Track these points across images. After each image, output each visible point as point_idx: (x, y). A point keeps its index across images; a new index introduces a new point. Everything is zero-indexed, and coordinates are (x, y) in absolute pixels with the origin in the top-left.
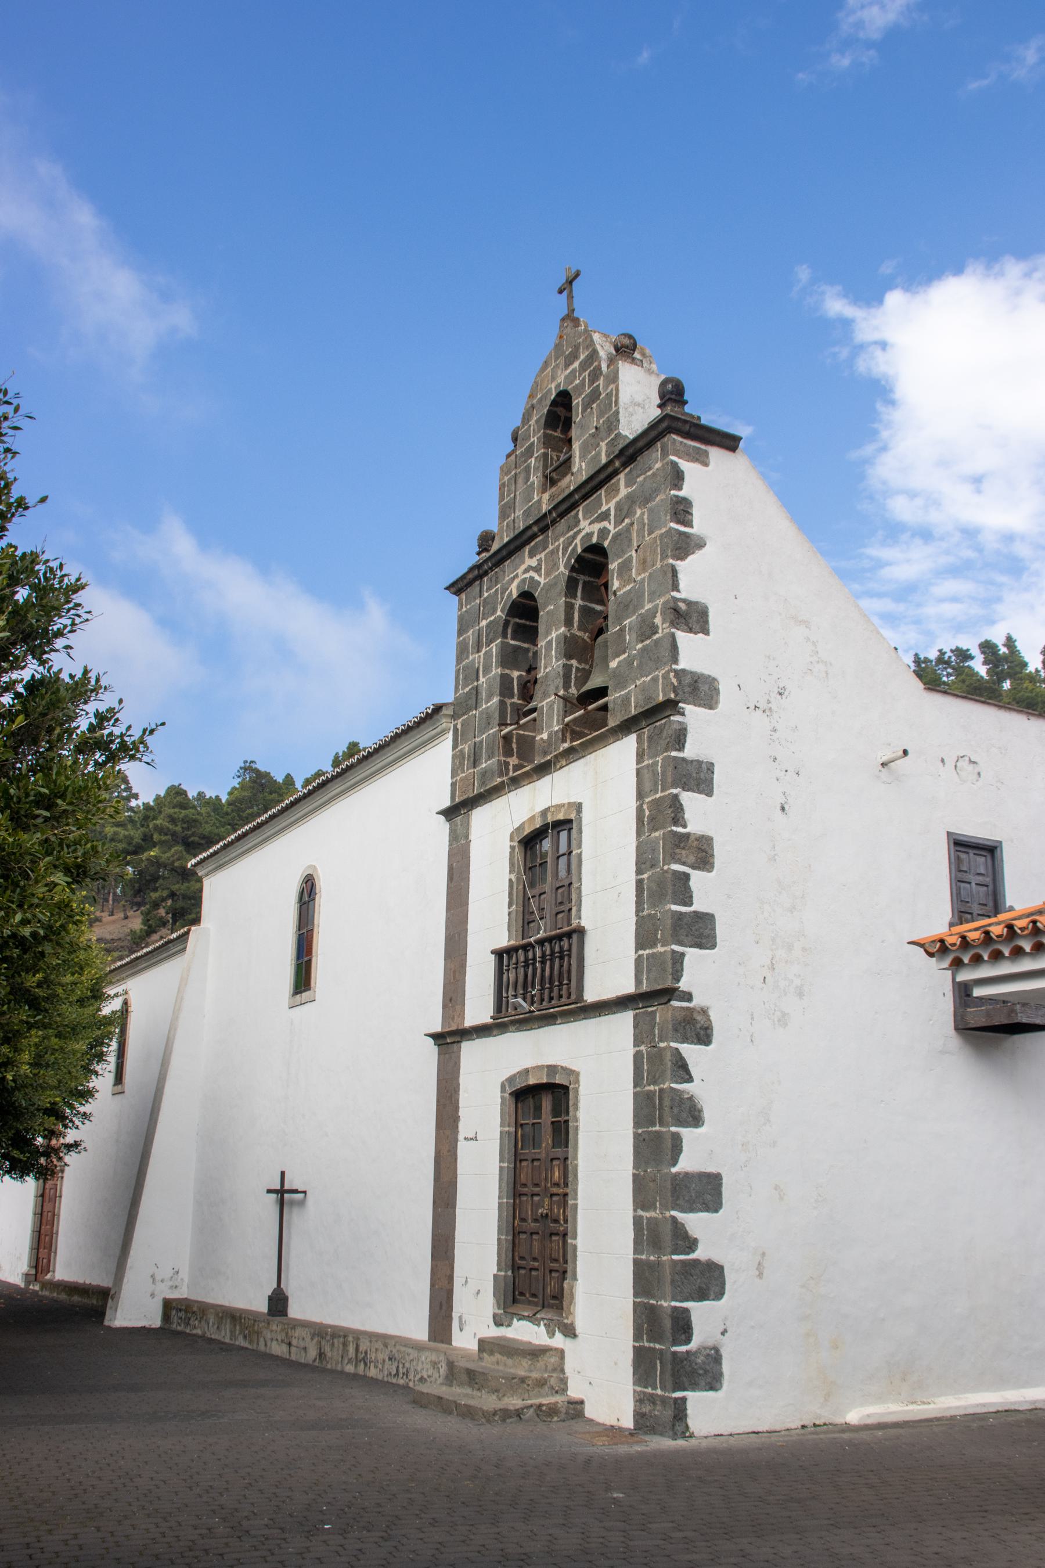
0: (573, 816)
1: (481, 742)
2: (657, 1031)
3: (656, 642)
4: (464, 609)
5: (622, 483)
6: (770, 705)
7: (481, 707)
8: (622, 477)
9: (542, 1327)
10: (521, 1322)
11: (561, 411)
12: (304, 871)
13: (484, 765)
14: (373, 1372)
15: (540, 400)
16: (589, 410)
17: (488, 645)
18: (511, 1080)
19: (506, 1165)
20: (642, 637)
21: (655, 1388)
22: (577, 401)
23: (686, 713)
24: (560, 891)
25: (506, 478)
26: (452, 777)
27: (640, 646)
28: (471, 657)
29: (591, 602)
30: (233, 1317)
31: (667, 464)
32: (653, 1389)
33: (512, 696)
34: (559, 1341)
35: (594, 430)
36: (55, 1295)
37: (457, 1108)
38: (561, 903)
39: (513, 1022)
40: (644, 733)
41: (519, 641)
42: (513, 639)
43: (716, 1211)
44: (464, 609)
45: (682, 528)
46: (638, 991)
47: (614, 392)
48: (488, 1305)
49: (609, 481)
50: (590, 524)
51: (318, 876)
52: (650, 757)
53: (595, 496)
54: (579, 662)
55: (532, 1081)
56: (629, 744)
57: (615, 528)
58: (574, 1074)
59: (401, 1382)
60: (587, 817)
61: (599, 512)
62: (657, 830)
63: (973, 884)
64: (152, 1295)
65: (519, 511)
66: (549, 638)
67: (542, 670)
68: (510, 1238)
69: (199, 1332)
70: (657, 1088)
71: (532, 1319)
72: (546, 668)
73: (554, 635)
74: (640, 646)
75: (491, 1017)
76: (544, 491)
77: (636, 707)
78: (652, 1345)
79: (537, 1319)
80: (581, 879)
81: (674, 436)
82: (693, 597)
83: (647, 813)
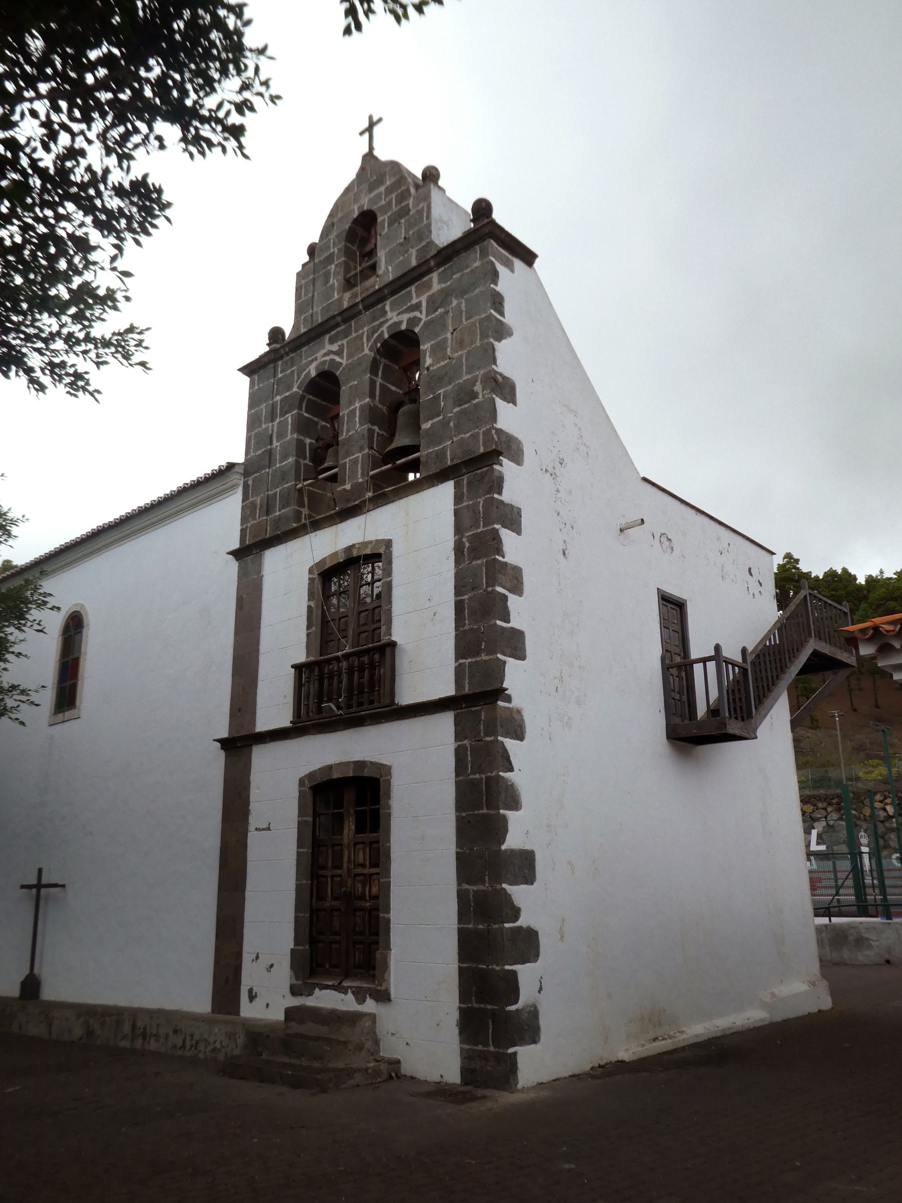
0: (382, 551)
1: (275, 494)
2: (482, 727)
3: (476, 405)
4: (256, 387)
7: (274, 466)
8: (435, 276)
9: (350, 996)
10: (325, 992)
11: (360, 231)
13: (278, 513)
14: (153, 1045)
15: (341, 220)
16: (396, 225)
17: (282, 415)
18: (311, 775)
20: (459, 402)
21: (487, 1045)
22: (383, 219)
23: (503, 464)
24: (363, 614)
25: (303, 282)
26: (241, 525)
28: (264, 426)
29: (388, 382)
31: (487, 262)
33: (305, 459)
34: (370, 1006)
39: (314, 726)
42: (306, 412)
44: (256, 387)
45: (499, 317)
46: (459, 694)
48: (284, 975)
50: (398, 315)
51: (87, 614)
52: (469, 499)
53: (404, 292)
54: (380, 429)
55: (335, 775)
56: (447, 490)
57: (427, 317)
58: (386, 770)
59: (188, 1053)
60: (397, 551)
61: (409, 304)
62: (479, 559)
63: (671, 630)
65: (317, 307)
66: (352, 407)
67: (344, 434)
68: (308, 915)
70: (483, 776)
71: (338, 988)
72: (348, 431)
73: (357, 405)
76: (345, 290)
77: (452, 460)
78: (482, 1006)
82: (506, 374)
83: (467, 545)
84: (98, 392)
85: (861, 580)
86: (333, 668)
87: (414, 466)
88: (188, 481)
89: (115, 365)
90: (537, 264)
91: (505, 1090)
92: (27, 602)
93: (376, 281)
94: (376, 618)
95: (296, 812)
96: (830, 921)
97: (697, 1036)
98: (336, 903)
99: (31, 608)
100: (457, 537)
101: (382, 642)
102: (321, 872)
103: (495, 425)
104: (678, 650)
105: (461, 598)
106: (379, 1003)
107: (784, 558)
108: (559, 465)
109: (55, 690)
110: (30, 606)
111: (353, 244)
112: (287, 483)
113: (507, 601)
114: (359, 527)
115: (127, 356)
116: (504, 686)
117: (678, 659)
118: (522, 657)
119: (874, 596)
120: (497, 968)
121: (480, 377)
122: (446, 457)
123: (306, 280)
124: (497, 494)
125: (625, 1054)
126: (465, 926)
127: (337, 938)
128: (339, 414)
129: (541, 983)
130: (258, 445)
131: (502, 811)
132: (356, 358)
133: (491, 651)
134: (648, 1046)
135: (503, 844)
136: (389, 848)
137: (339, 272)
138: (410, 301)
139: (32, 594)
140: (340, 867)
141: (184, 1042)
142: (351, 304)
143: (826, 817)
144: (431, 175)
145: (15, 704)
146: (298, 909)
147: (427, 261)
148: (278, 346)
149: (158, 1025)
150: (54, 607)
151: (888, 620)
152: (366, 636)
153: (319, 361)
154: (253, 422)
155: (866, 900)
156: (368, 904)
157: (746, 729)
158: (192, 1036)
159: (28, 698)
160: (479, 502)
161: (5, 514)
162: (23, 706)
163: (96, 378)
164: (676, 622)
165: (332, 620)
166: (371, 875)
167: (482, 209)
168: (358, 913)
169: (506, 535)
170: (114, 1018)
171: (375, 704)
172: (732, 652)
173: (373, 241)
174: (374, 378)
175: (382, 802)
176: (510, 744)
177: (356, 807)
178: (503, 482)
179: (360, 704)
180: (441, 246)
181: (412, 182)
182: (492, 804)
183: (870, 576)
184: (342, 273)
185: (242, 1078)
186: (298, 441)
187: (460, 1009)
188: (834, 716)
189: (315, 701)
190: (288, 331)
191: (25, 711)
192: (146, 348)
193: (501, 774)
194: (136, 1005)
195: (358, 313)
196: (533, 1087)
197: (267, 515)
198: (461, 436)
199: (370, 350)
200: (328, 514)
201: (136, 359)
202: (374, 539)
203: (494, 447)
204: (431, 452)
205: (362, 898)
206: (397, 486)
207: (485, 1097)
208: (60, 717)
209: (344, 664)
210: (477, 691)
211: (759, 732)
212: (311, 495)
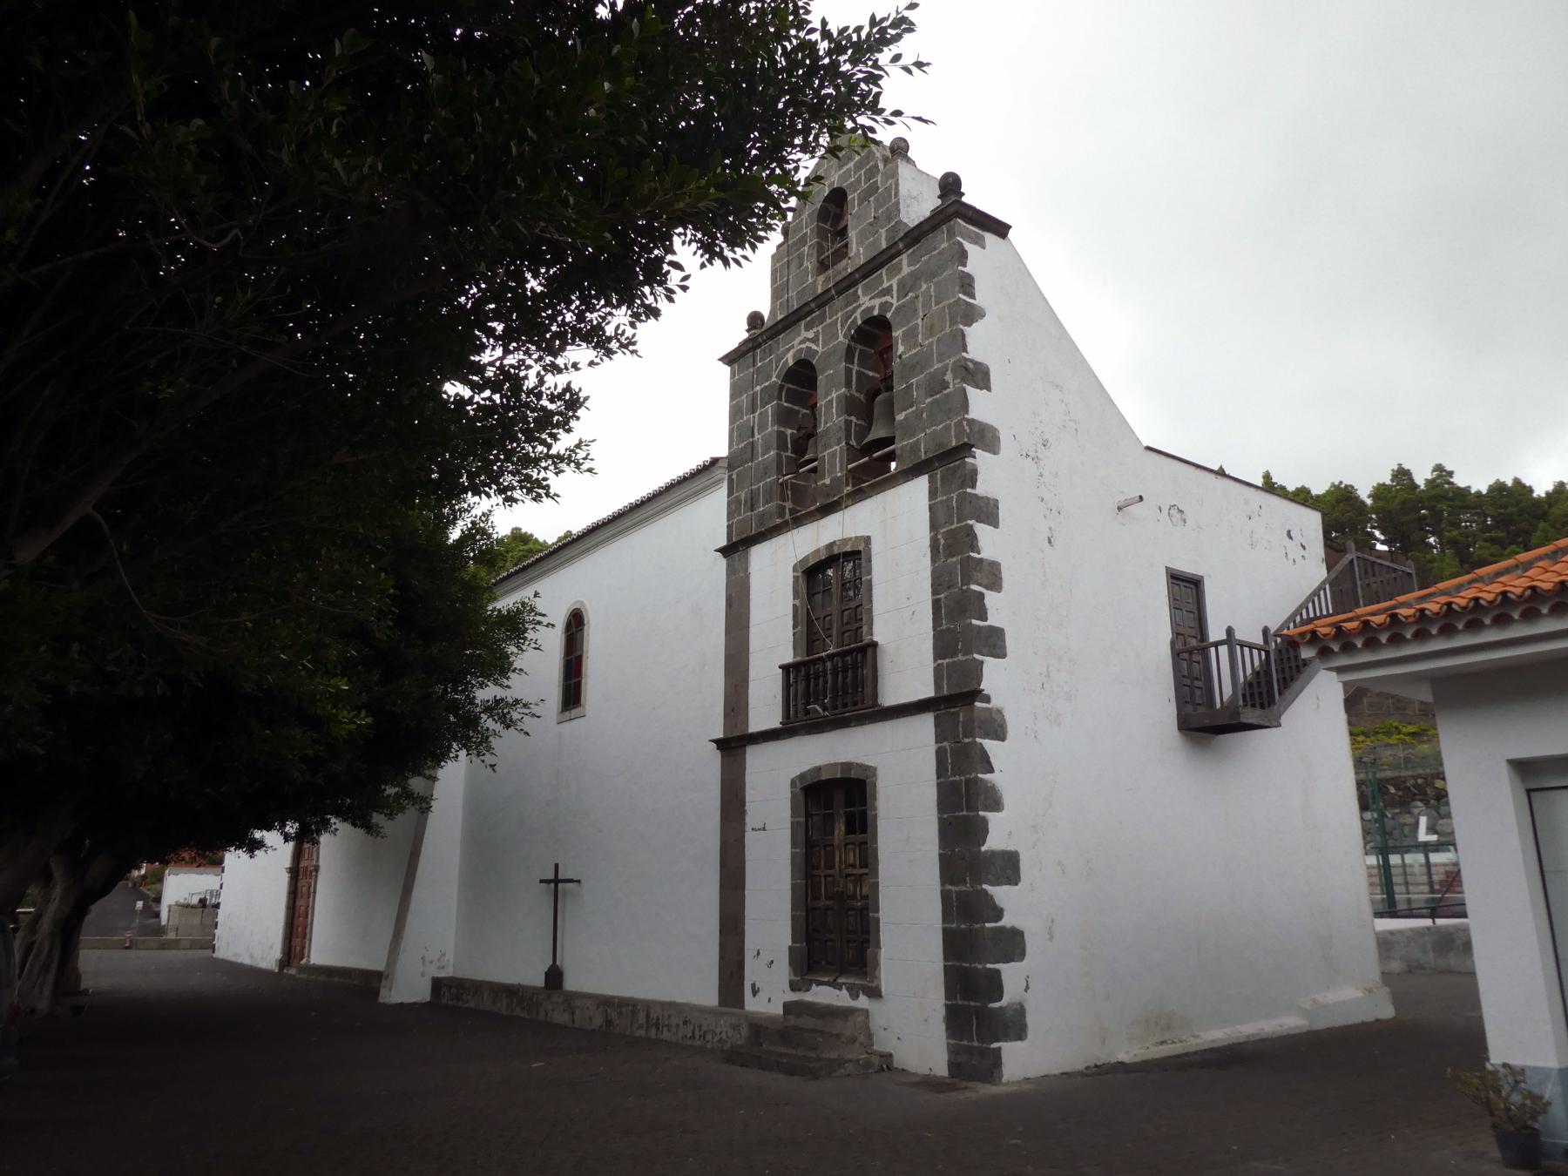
2: (960, 729)
4: (737, 377)
5: (905, 262)
8: (904, 258)
9: (844, 991)
11: (832, 208)
14: (666, 1035)
17: (763, 406)
18: (802, 776)
19: (798, 850)
22: (852, 196)
24: (846, 613)
25: (778, 265)
26: (728, 520)
27: (929, 400)
28: (745, 418)
30: (512, 992)
31: (954, 243)
34: (863, 1002)
35: (873, 219)
36: (313, 977)
38: (847, 624)
40: (937, 474)
41: (791, 403)
43: (1017, 884)
44: (737, 377)
46: (938, 695)
47: (893, 186)
54: (857, 419)
55: (824, 777)
56: (921, 484)
57: (898, 302)
58: (872, 771)
59: (699, 1043)
60: (875, 547)
61: (880, 289)
62: (954, 556)
64: (423, 975)
65: (793, 292)
67: (822, 426)
68: (804, 914)
69: (472, 1004)
70: (963, 778)
71: (835, 985)
72: (826, 423)
73: (834, 395)
74: (929, 400)
75: (781, 723)
76: (819, 274)
77: (925, 453)
78: (966, 1003)
79: (838, 984)
82: (978, 359)
83: (942, 542)
84: (558, 496)
89: (569, 470)
90: (1011, 234)
91: (990, 1083)
93: (848, 264)
94: (859, 617)
95: (789, 813)
96: (1434, 922)
97: (1213, 1041)
98: (829, 903)
99: (527, 629)
102: (815, 872)
103: (966, 416)
104: (1193, 632)
106: (872, 1000)
107: (1434, 471)
108: (1043, 448)
109: (561, 688)
112: (769, 477)
114: (840, 522)
115: (578, 465)
116: (981, 687)
117: (1193, 643)
118: (1003, 655)
119: (1556, 511)
120: (979, 966)
121: (950, 366)
122: (920, 450)
125: (1124, 1056)
127: (832, 936)
128: (816, 404)
130: (741, 437)
131: (981, 813)
132: (831, 346)
133: (968, 652)
136: (876, 849)
137: (812, 254)
140: (832, 867)
141: (693, 1033)
145: (520, 716)
148: (758, 331)
150: (549, 624)
151: (1370, 611)
153: (795, 350)
154: (735, 414)
156: (859, 904)
157: (1266, 717)
158: (700, 1026)
160: (953, 497)
163: (555, 482)
164: (1191, 601)
165: (816, 619)
166: (862, 875)
167: (950, 185)
168: (850, 913)
169: (982, 530)
170: (630, 1008)
174: (850, 366)
176: (989, 745)
178: (977, 475)
179: (845, 705)
180: (912, 225)
185: (742, 1066)
187: (946, 1005)
190: (766, 315)
191: (528, 723)
192: (592, 460)
197: (752, 511)
199: (845, 336)
201: (584, 467)
202: (853, 535)
205: (853, 897)
207: (966, 1088)
208: (567, 714)
209: (829, 664)
210: (953, 693)
211: (1283, 720)
212: (795, 488)
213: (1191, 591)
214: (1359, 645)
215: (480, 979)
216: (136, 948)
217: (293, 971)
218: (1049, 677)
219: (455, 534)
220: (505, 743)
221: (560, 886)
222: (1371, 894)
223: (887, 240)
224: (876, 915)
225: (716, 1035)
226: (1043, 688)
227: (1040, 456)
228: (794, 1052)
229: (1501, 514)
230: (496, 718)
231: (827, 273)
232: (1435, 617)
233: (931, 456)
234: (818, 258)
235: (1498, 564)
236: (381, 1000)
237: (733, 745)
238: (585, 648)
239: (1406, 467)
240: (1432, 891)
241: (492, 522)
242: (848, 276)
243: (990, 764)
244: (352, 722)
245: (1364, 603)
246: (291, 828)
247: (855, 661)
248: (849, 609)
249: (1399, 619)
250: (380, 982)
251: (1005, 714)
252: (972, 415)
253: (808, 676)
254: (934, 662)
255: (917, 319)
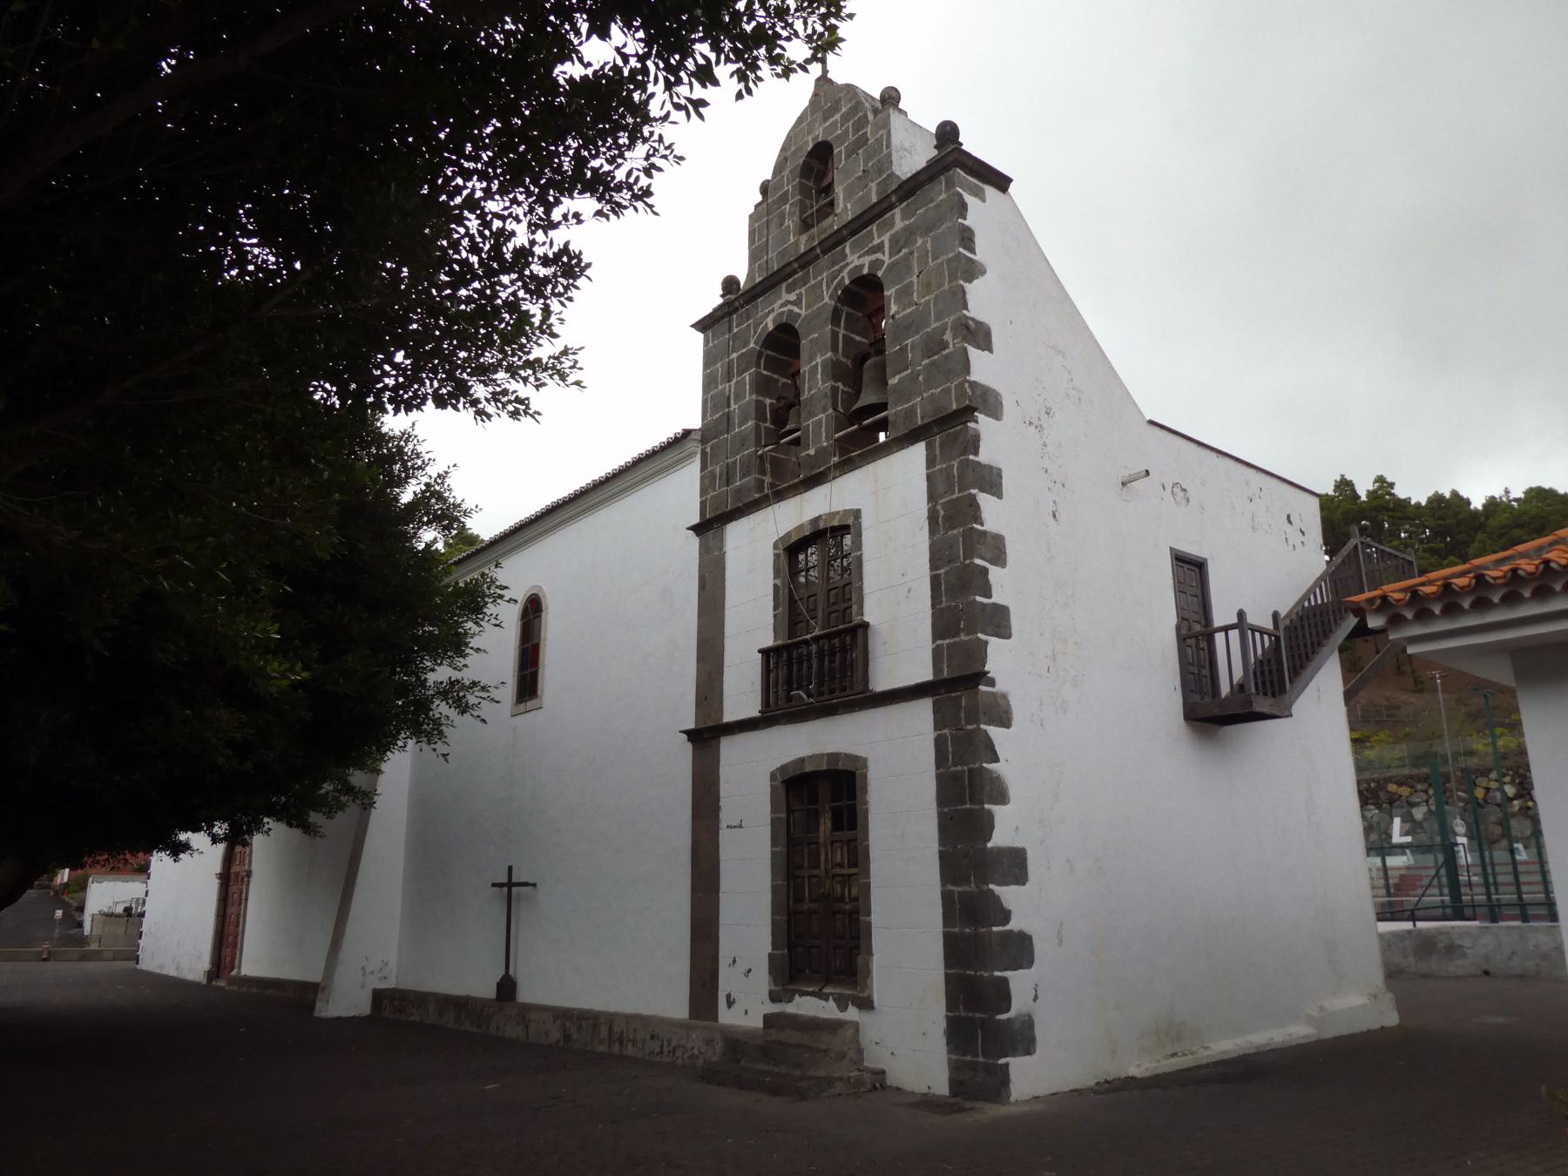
0: (850, 522)
1: (735, 462)
2: (963, 715)
3: (947, 357)
4: (711, 345)
6: (1041, 422)
7: (732, 431)
8: (897, 212)
9: (832, 1003)
10: (804, 998)
11: (816, 165)
12: (529, 590)
13: (738, 483)
14: (630, 1051)
17: (740, 374)
18: (783, 769)
19: (779, 849)
20: (928, 353)
21: (977, 1056)
23: (979, 421)
24: (832, 592)
25: (756, 225)
27: (927, 361)
28: (720, 387)
32: (972, 1057)
33: (766, 421)
34: (852, 1014)
36: (245, 989)
37: (717, 799)
38: (834, 604)
40: (935, 440)
41: (770, 371)
44: (711, 345)
45: (968, 254)
46: (937, 679)
47: (885, 137)
48: (762, 981)
49: (882, 216)
50: (859, 257)
51: (544, 596)
53: (864, 231)
54: (844, 386)
55: (808, 769)
56: (918, 452)
57: (890, 258)
58: (862, 762)
59: (667, 1059)
60: (866, 522)
61: (870, 245)
62: (955, 528)
67: (806, 393)
68: (785, 918)
69: (415, 1018)
70: (965, 768)
72: (810, 390)
73: (819, 360)
74: (927, 361)
75: (760, 712)
76: (801, 233)
77: (922, 418)
78: (970, 1014)
79: (825, 994)
80: (862, 579)
81: (958, 170)
82: (980, 318)
83: (942, 513)
84: (539, 414)
85: (1477, 503)
86: (802, 652)
87: (883, 425)
88: (643, 451)
89: (552, 384)
90: (1012, 189)
92: (484, 596)
93: (834, 221)
94: (847, 597)
95: (769, 808)
96: (1415, 925)
97: (1225, 1052)
98: (813, 906)
99: (487, 603)
100: (930, 505)
101: (854, 623)
102: (798, 873)
103: (968, 378)
104: (1197, 617)
105: (937, 572)
107: (1375, 482)
108: (1046, 415)
109: (516, 677)
110: (486, 599)
111: (808, 180)
112: (747, 449)
113: (988, 573)
114: (825, 496)
115: (563, 377)
116: (987, 668)
117: (1198, 628)
118: (1008, 636)
119: (1493, 523)
120: (986, 974)
121: (950, 324)
123: (760, 223)
124: (972, 454)
126: (950, 930)
128: (799, 370)
129: (1036, 991)
130: (715, 408)
131: (986, 806)
134: (1164, 1062)
135: (989, 841)
137: (794, 213)
138: (871, 242)
139: (489, 588)
141: (662, 1046)
142: (808, 248)
143: (1427, 802)
144: (891, 98)
145: (476, 701)
146: (775, 910)
147: (888, 196)
148: (732, 297)
149: (635, 1030)
150: (511, 599)
151: (1401, 587)
152: (837, 616)
153: (776, 313)
154: (709, 383)
155: (1461, 901)
156: (847, 907)
158: (669, 1041)
159: (488, 694)
161: (459, 505)
162: (485, 704)
163: (537, 399)
164: (1194, 584)
166: (850, 875)
167: (948, 134)
168: (837, 917)
170: (591, 1021)
171: (848, 691)
172: (1260, 617)
173: (830, 174)
175: (859, 797)
176: (994, 732)
177: (832, 802)
179: (832, 691)
181: (869, 107)
182: (977, 798)
183: (1493, 498)
184: (797, 213)
186: (758, 402)
187: (947, 1017)
188: (1433, 678)
189: (785, 688)
190: (742, 279)
191: (486, 709)
192: (580, 369)
193: (985, 765)
194: (613, 1009)
195: (815, 258)
196: (1027, 1100)
197: (728, 486)
198: (931, 391)
199: (831, 297)
200: (791, 483)
201: (571, 379)
202: (841, 509)
203: (967, 402)
204: (899, 411)
205: (841, 899)
206: (865, 450)
207: (972, 1109)
208: (522, 706)
209: (814, 648)
210: (955, 675)
211: (1294, 709)
212: (774, 461)
213: (1194, 574)
214: (1437, 611)
215: (612, 1010)
216: (54, 960)
217: (222, 983)
218: (1055, 660)
219: (406, 497)
220: (459, 728)
221: (514, 889)
222: (1374, 897)
223: (878, 194)
224: (867, 919)
225: (687, 1050)
226: (1048, 671)
227: (1044, 425)
228: (776, 1069)
229: (1440, 525)
230: (450, 701)
231: (810, 232)
232: (1530, 577)
233: (930, 420)
234: (801, 216)
235: (1533, 542)
236: (317, 1014)
237: (706, 736)
238: (542, 636)
239: (1348, 478)
240: (1389, 895)
241: (449, 485)
242: (835, 233)
243: (995, 753)
244: (283, 676)
245: (1368, 588)
246: (220, 829)
247: (843, 642)
248: (834, 588)
249: (1485, 580)
250: (317, 994)
251: (1009, 699)
252: (973, 377)
253: (790, 659)
254: (933, 643)
255: (912, 276)
